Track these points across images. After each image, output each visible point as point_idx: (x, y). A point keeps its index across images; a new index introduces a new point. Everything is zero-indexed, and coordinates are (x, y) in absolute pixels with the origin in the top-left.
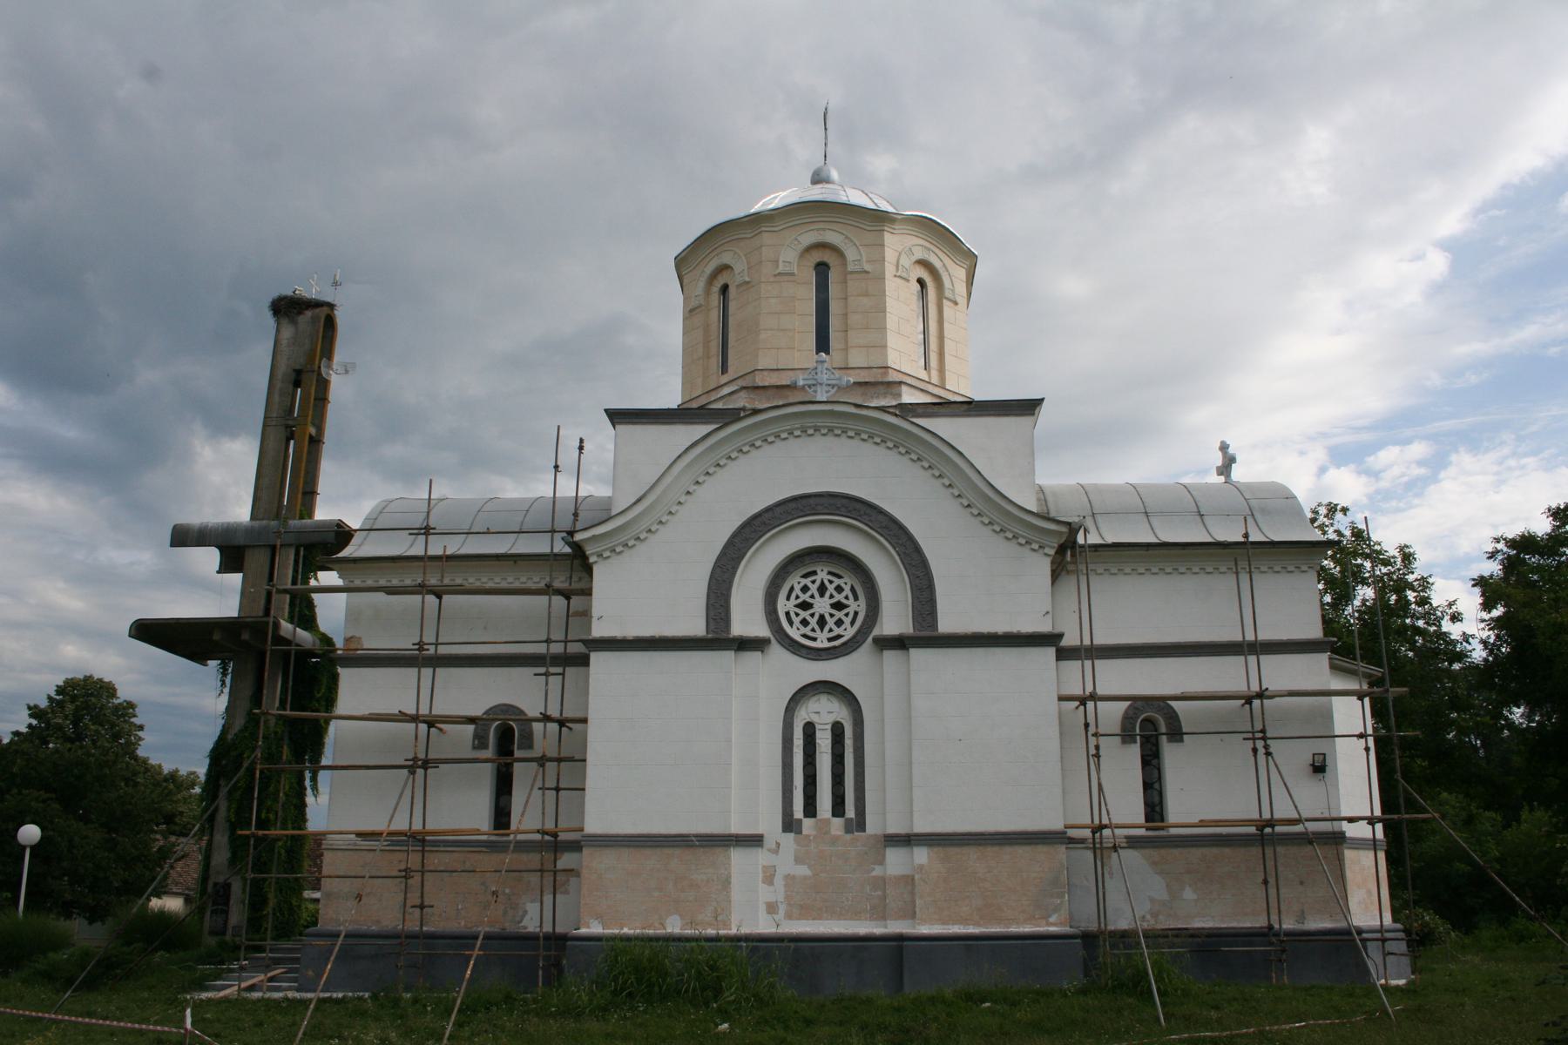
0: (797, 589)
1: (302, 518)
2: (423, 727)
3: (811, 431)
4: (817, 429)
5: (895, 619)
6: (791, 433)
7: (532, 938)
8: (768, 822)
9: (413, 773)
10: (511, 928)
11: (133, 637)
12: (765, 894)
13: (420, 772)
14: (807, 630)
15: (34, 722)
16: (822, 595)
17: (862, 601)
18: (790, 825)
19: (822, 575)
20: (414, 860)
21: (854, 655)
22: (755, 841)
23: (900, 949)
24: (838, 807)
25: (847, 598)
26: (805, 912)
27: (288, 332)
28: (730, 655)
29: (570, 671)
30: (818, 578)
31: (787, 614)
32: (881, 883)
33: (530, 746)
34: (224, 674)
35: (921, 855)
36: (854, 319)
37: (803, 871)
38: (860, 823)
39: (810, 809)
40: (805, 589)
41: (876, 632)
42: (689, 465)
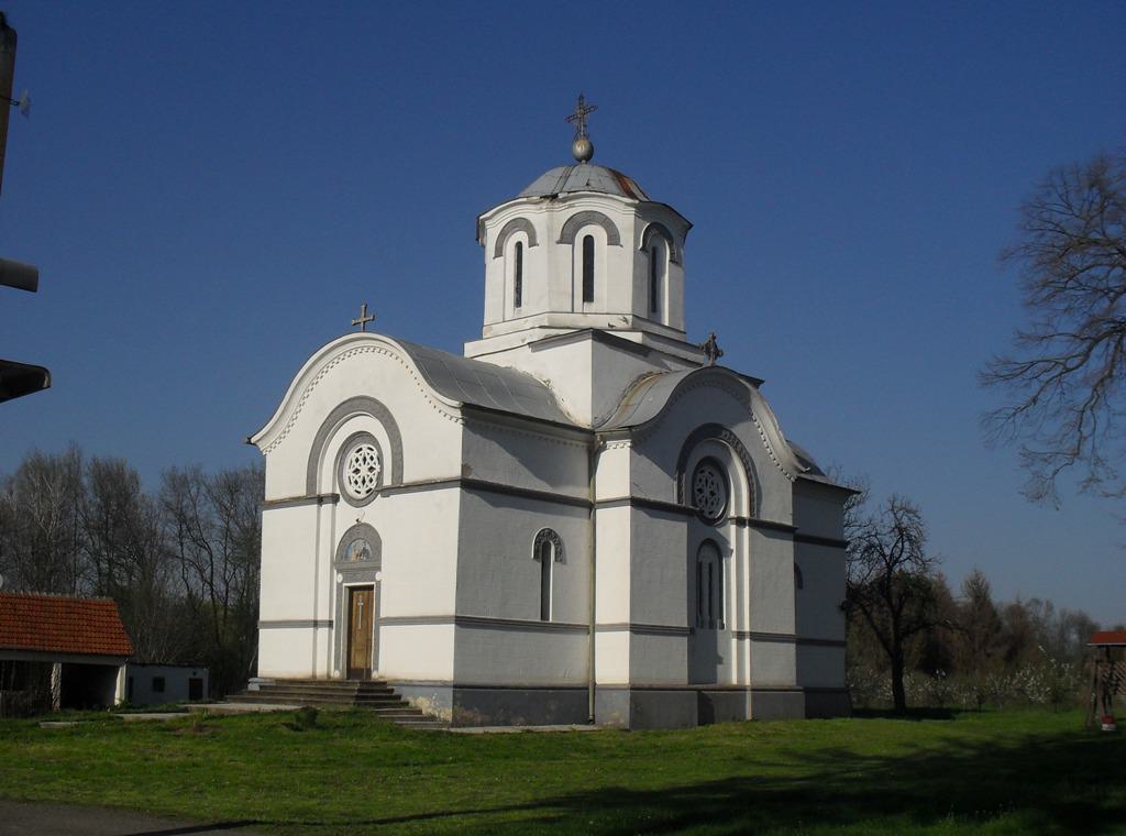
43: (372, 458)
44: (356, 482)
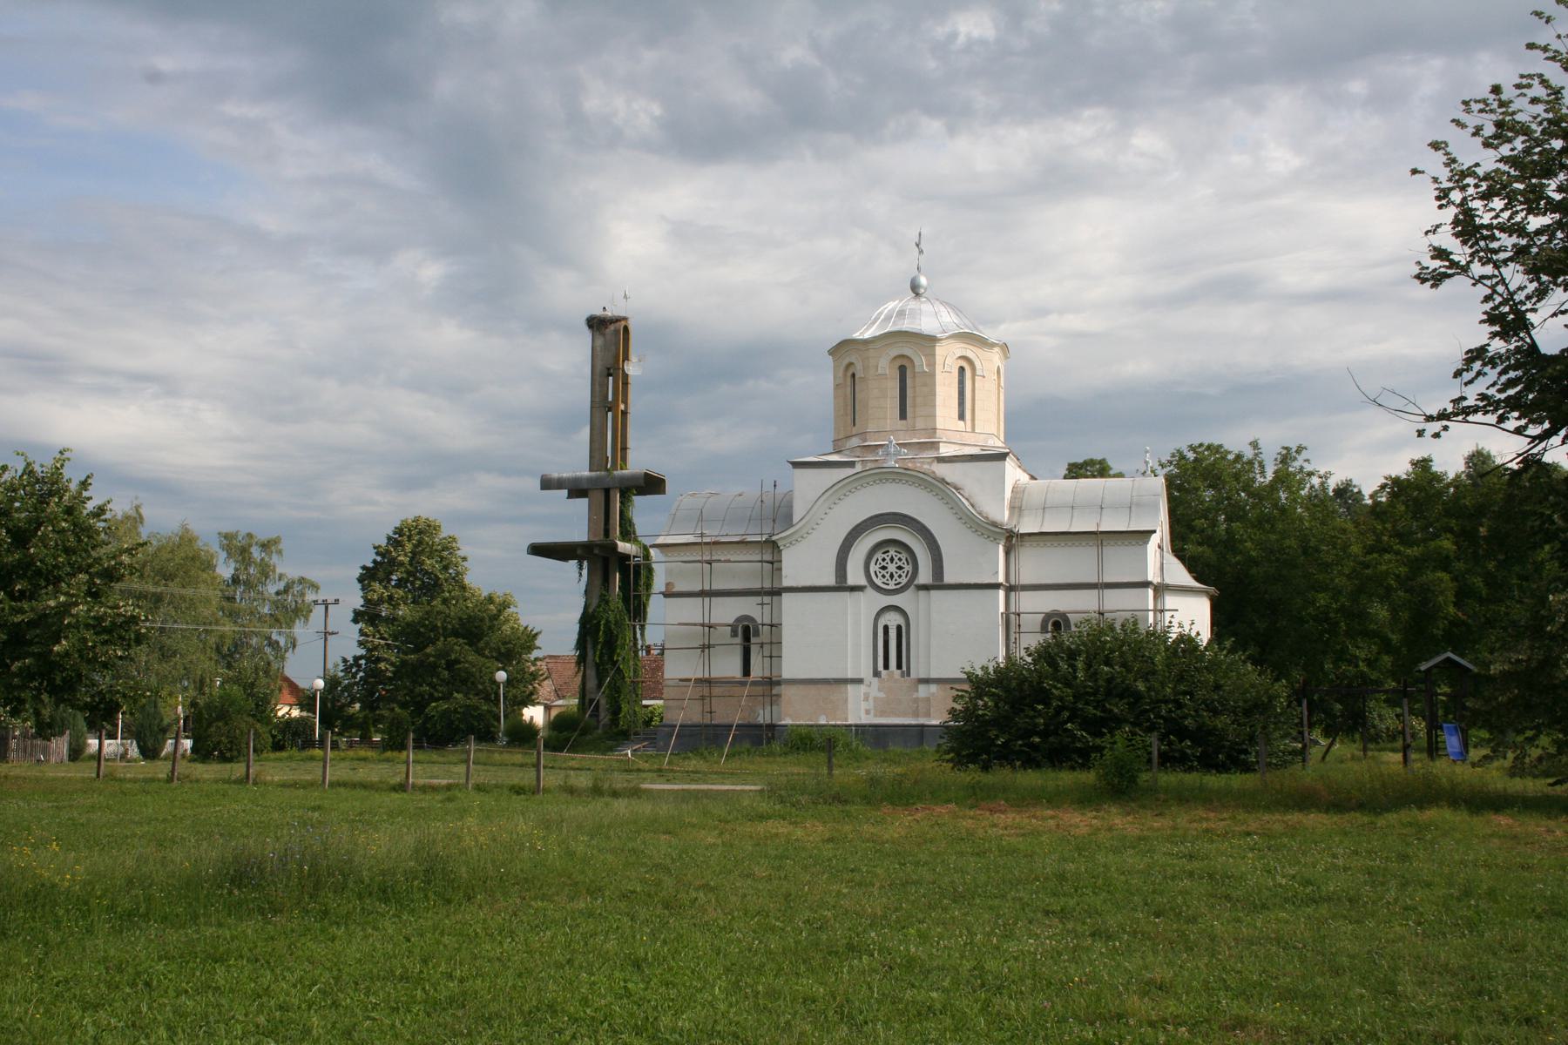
1: (622, 469)
2: (707, 629)
4: (887, 480)
5: (925, 576)
7: (761, 726)
8: (865, 671)
9: (703, 651)
10: (752, 721)
12: (864, 705)
13: (707, 650)
14: (885, 580)
15: (379, 559)
18: (876, 674)
19: (892, 553)
20: (706, 691)
21: (906, 593)
22: (859, 681)
23: (922, 732)
24: (899, 666)
26: (882, 713)
27: (600, 341)
28: (848, 593)
29: (775, 598)
30: (890, 554)
32: (916, 700)
33: (758, 635)
34: (581, 568)
35: (933, 688)
36: (919, 400)
37: (882, 695)
38: (909, 675)
39: (886, 666)
40: (884, 560)
41: (916, 583)
42: (831, 495)
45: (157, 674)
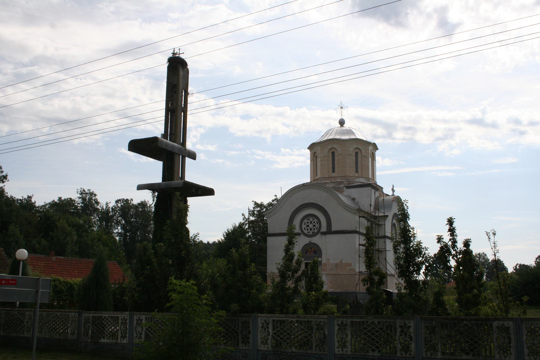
0: (306, 222)
3: (272, 216)
6: (301, 190)
11: (367, 143)
16: (311, 224)
17: (318, 225)
19: (311, 219)
25: (309, 228)
31: (304, 228)
43: (314, 222)
44: (308, 229)
45: (448, 291)
